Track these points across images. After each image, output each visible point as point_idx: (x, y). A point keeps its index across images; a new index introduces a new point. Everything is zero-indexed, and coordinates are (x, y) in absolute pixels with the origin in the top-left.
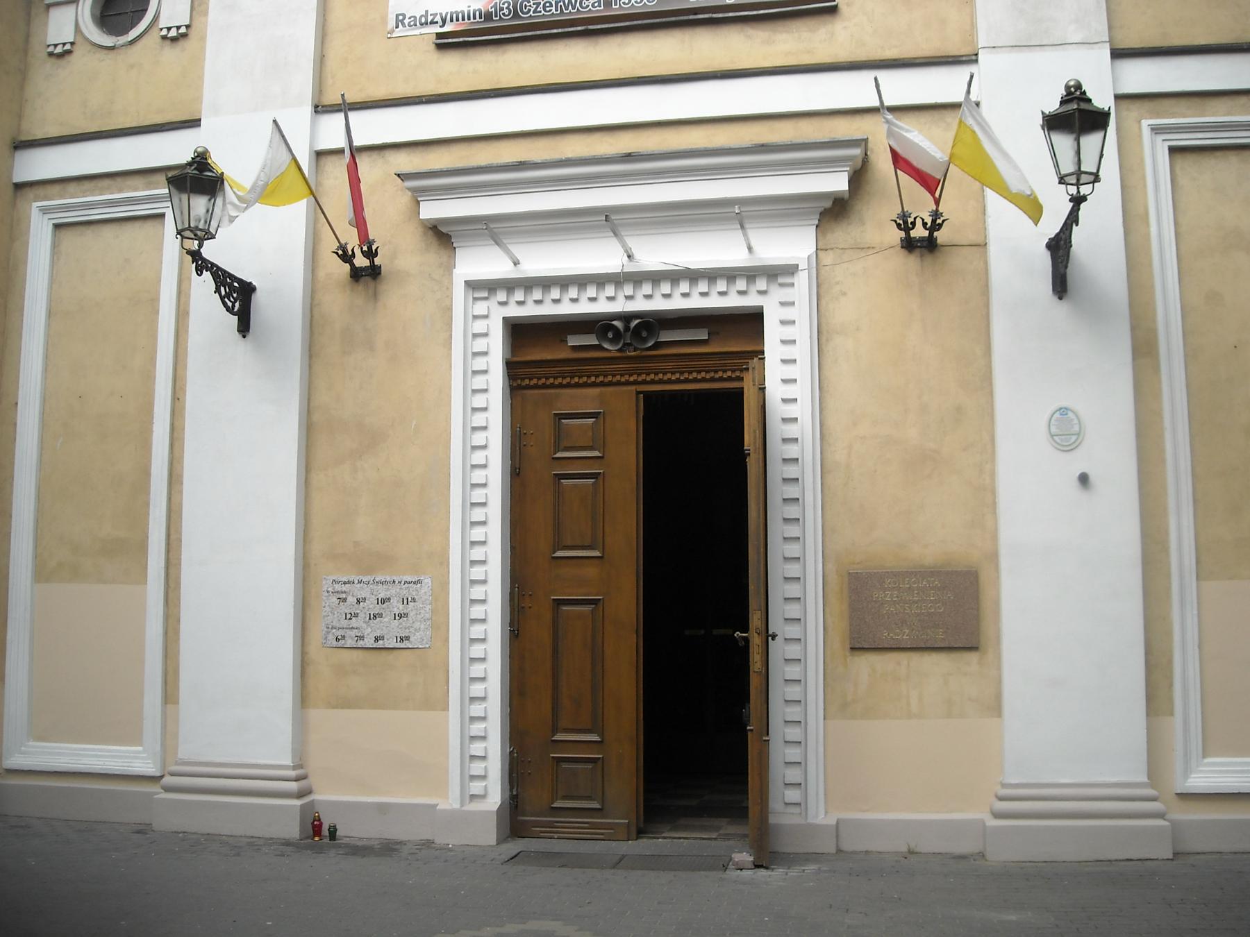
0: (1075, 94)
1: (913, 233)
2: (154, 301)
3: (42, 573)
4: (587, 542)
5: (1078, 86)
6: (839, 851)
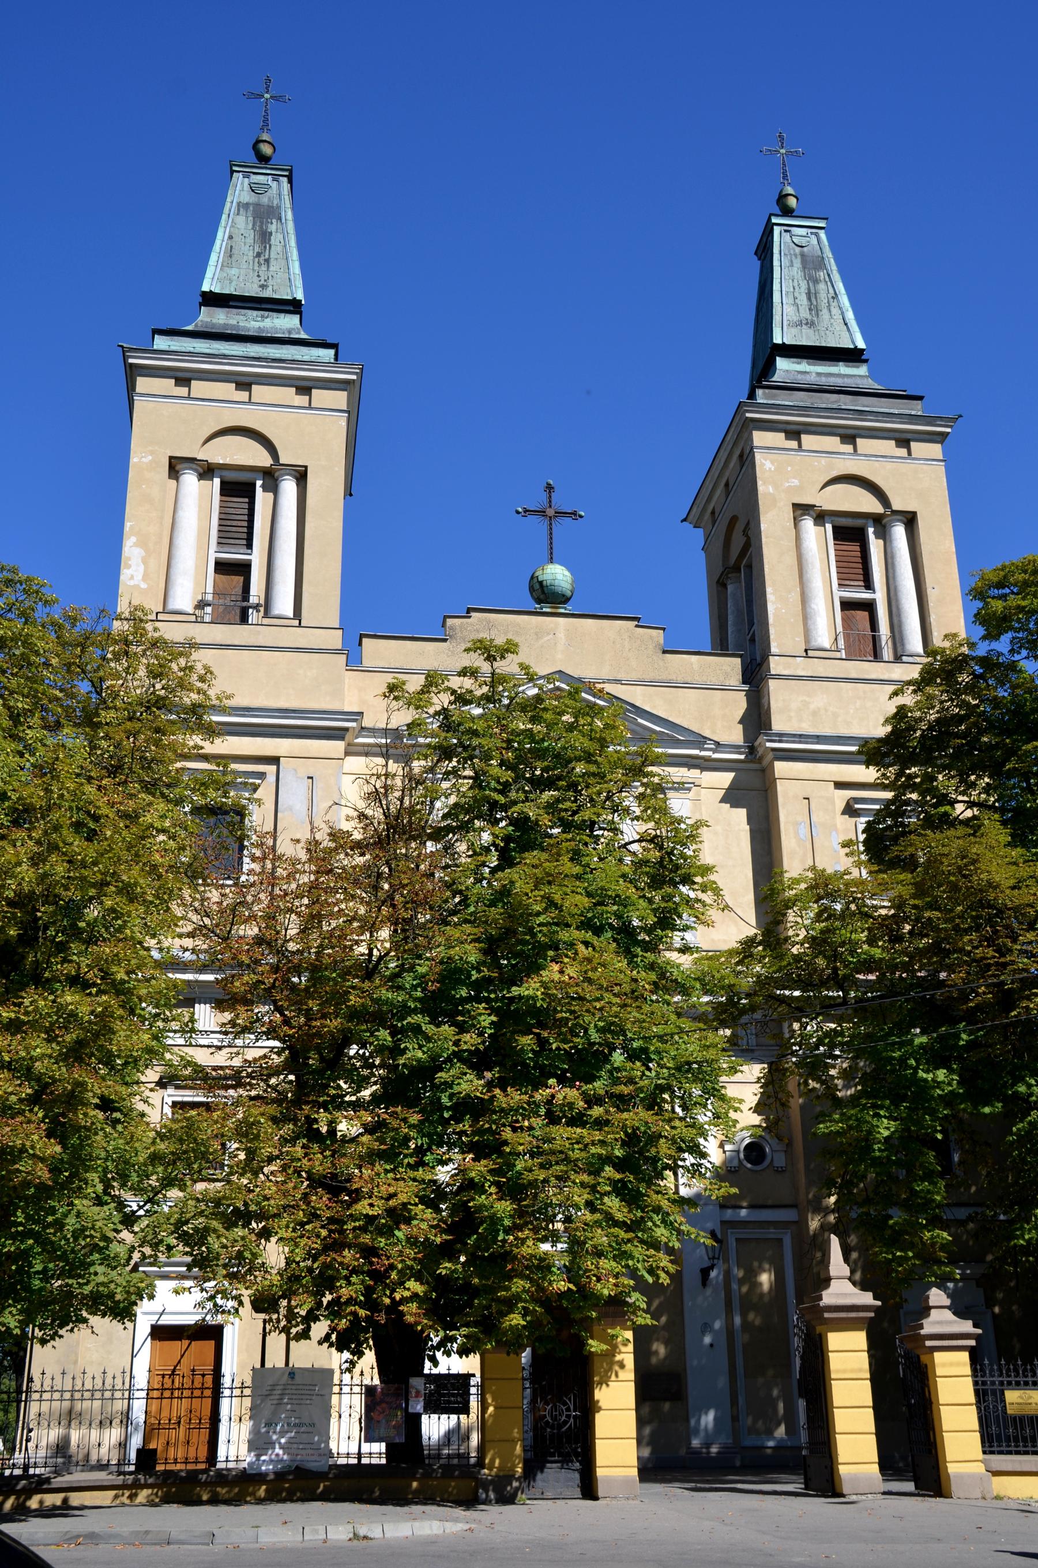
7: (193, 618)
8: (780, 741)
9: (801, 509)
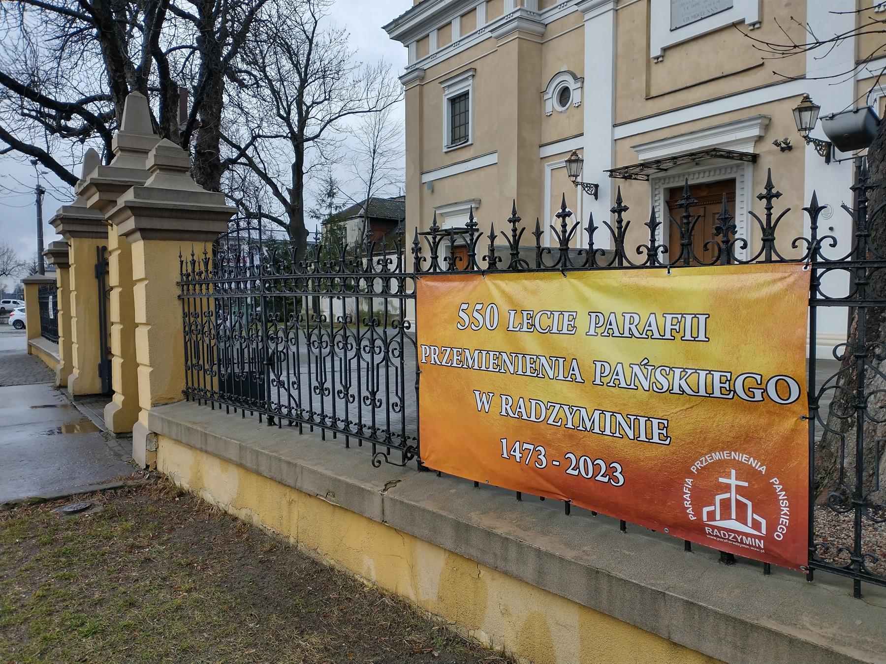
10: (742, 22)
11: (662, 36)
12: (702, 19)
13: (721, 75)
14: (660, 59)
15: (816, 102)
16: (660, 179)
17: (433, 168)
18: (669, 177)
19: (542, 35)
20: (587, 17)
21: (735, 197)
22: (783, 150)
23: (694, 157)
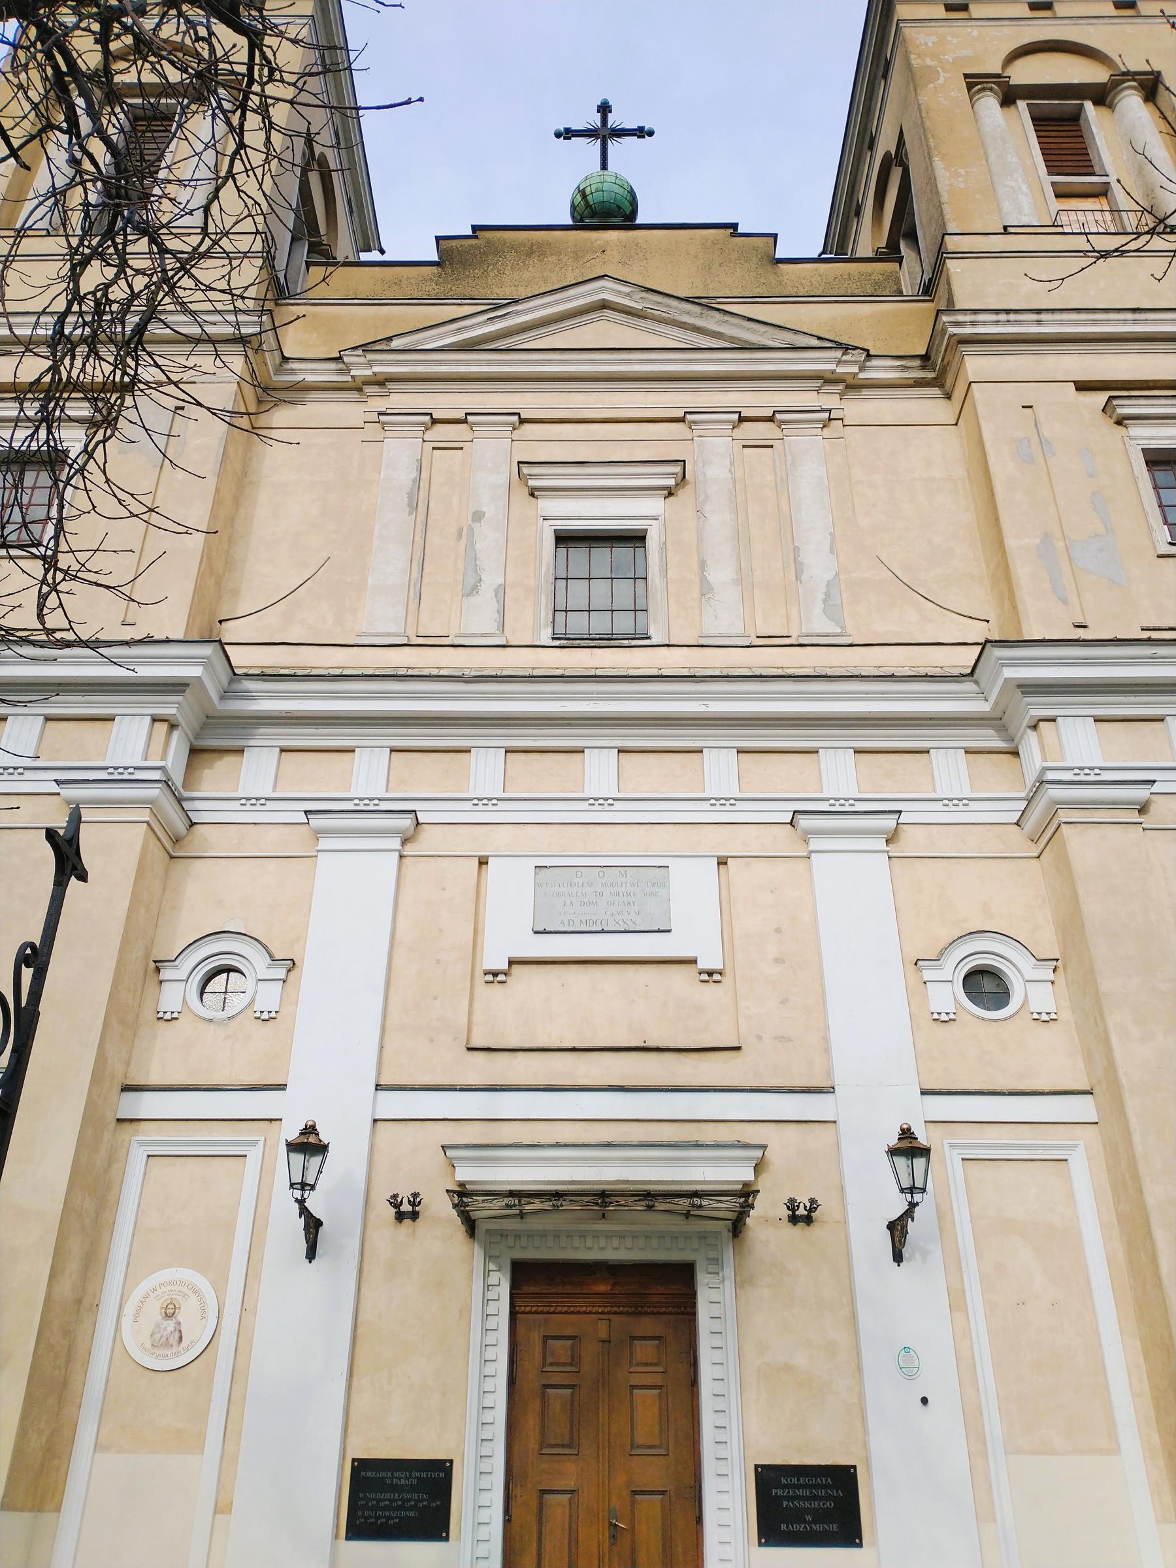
0: (906, 1133)
1: (402, 1209)
2: (230, 1227)
3: (98, 1447)
4: (566, 1442)
5: (909, 1129)
6: (161, 982)
7: (44, 233)
8: (973, 324)
9: (975, 82)
10: (694, 961)
11: (508, 935)
12: (603, 932)
13: (641, 1044)
14: (501, 978)
15: (324, 1137)
16: (503, 1234)
17: (154, 1080)
18: (531, 1235)
19: (177, 840)
20: (324, 844)
21: (694, 1305)
22: (794, 1219)
23: (602, 1198)
